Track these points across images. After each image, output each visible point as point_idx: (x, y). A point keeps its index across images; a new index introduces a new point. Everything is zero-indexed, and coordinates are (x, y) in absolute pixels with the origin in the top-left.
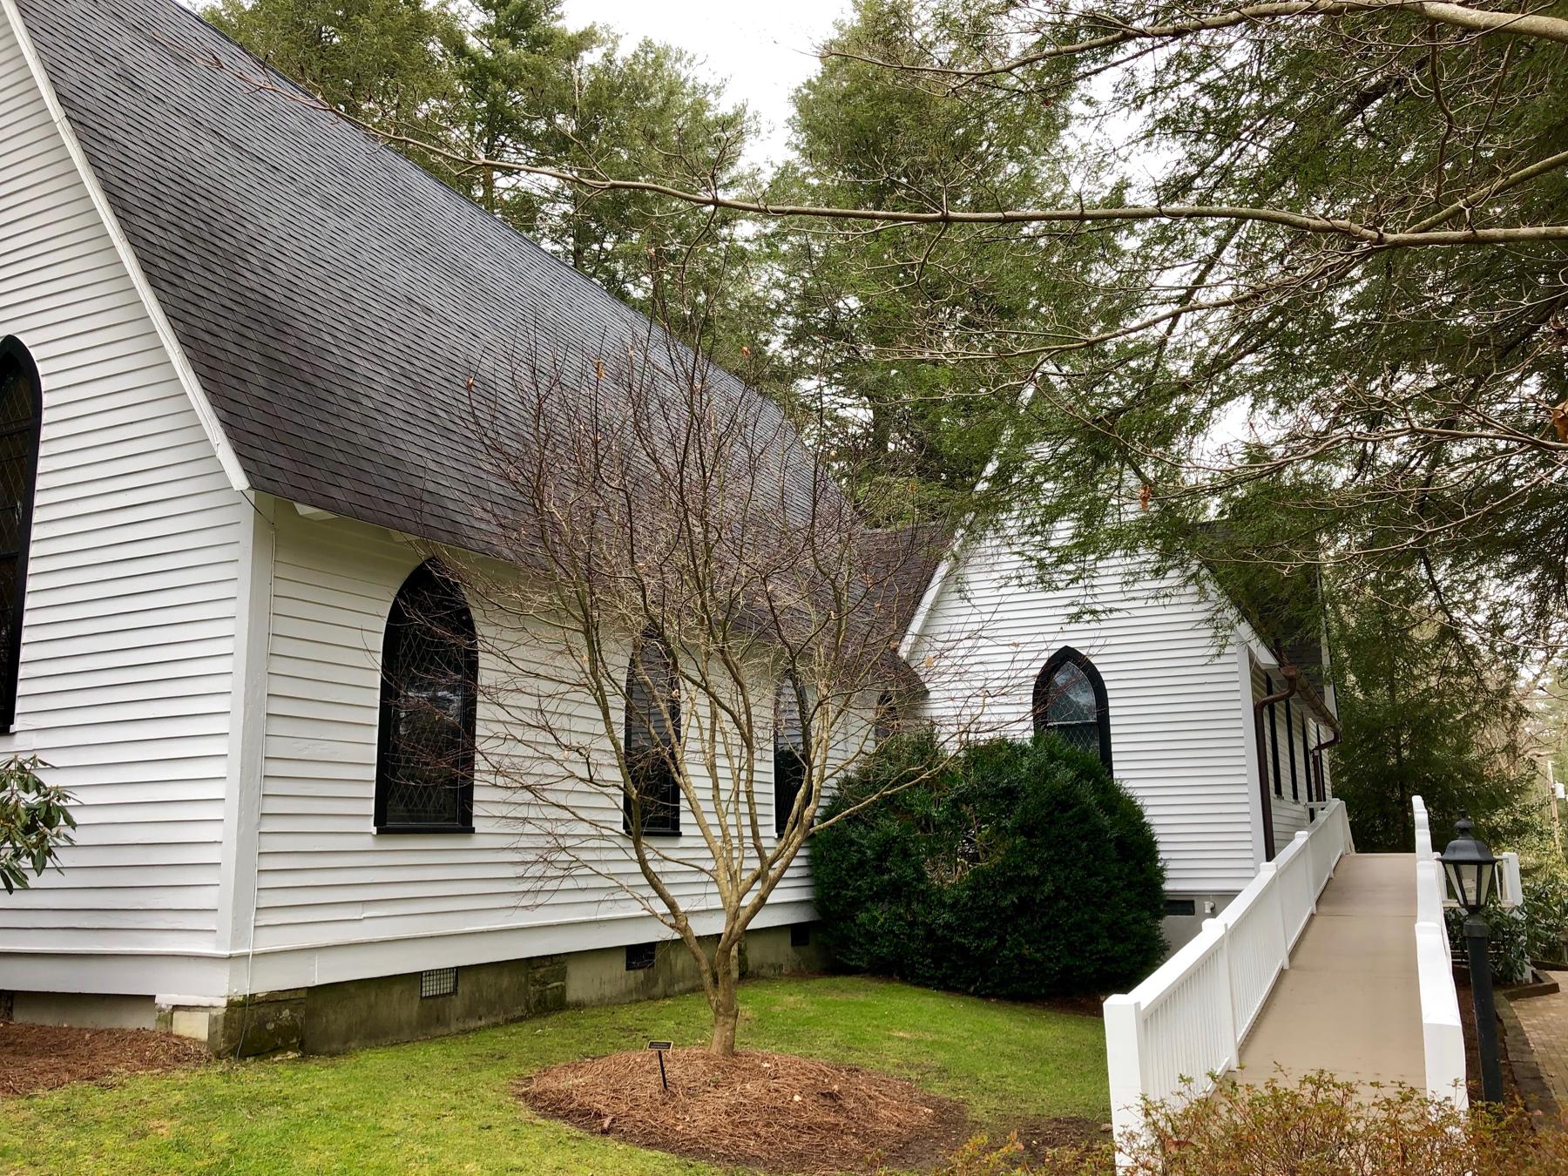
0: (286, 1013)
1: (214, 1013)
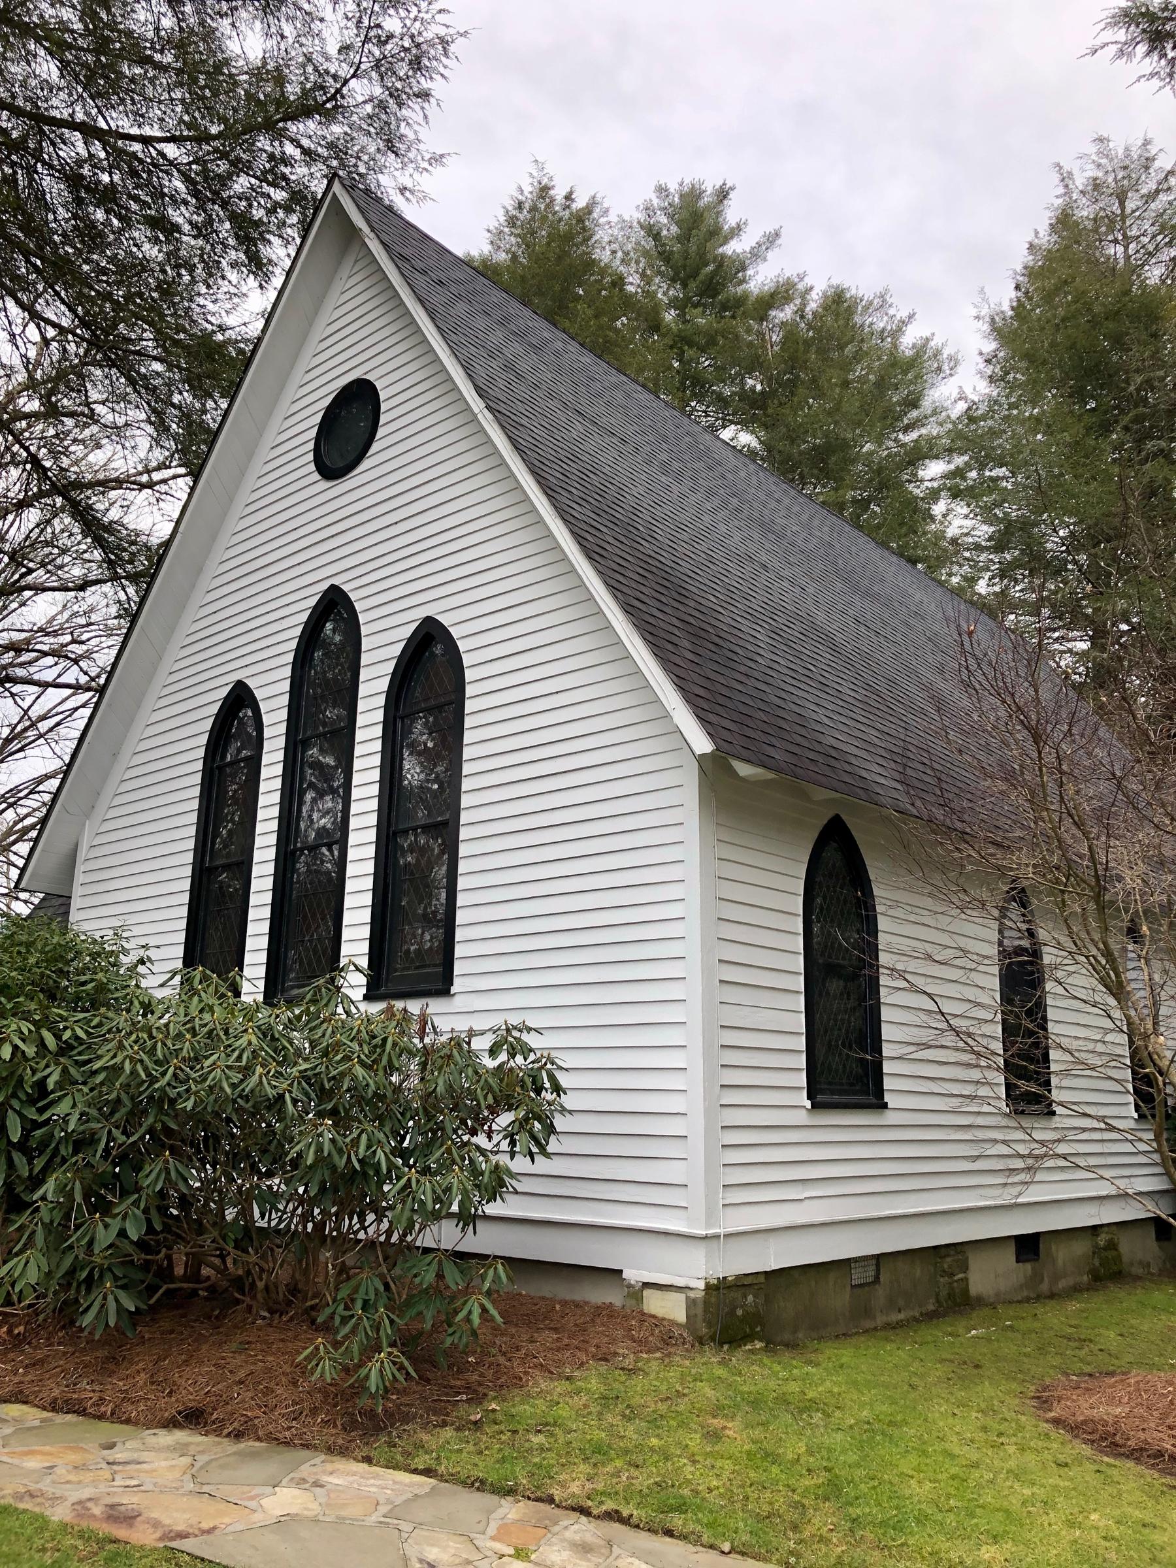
0: (750, 1298)
1: (692, 1294)
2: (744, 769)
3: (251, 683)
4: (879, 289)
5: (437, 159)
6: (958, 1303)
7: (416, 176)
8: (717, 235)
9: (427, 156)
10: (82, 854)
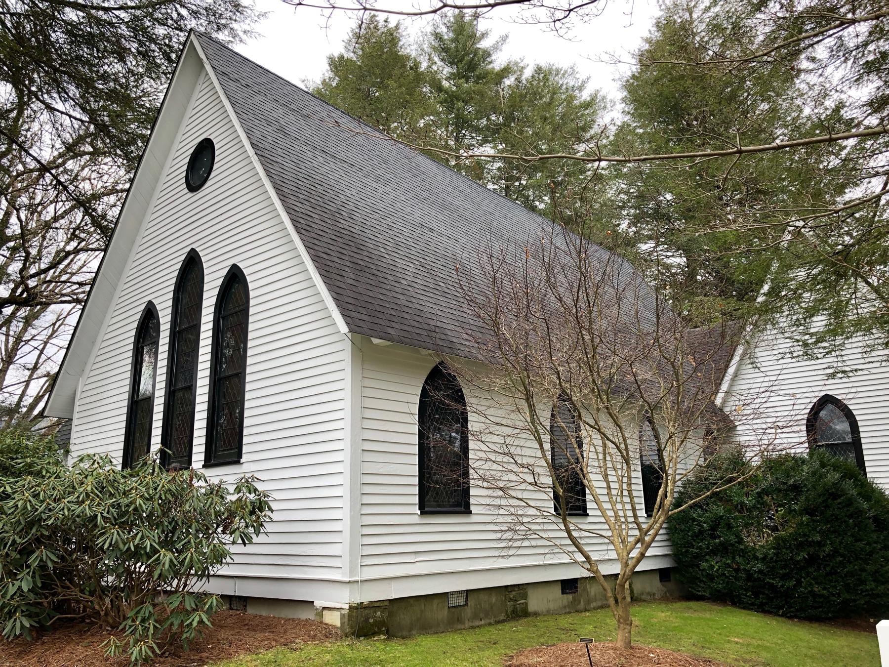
0: (379, 613)
1: (343, 612)
2: (376, 341)
3: (155, 302)
4: (570, 64)
5: (264, 15)
6: (520, 613)
7: (252, 24)
8: (473, 37)
9: (257, 14)
10: (78, 396)
